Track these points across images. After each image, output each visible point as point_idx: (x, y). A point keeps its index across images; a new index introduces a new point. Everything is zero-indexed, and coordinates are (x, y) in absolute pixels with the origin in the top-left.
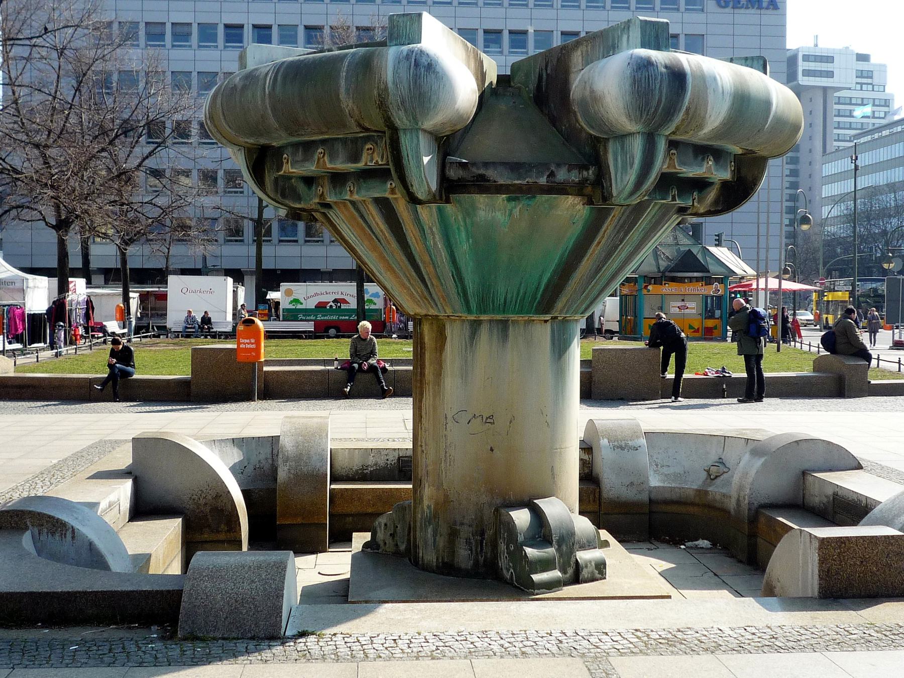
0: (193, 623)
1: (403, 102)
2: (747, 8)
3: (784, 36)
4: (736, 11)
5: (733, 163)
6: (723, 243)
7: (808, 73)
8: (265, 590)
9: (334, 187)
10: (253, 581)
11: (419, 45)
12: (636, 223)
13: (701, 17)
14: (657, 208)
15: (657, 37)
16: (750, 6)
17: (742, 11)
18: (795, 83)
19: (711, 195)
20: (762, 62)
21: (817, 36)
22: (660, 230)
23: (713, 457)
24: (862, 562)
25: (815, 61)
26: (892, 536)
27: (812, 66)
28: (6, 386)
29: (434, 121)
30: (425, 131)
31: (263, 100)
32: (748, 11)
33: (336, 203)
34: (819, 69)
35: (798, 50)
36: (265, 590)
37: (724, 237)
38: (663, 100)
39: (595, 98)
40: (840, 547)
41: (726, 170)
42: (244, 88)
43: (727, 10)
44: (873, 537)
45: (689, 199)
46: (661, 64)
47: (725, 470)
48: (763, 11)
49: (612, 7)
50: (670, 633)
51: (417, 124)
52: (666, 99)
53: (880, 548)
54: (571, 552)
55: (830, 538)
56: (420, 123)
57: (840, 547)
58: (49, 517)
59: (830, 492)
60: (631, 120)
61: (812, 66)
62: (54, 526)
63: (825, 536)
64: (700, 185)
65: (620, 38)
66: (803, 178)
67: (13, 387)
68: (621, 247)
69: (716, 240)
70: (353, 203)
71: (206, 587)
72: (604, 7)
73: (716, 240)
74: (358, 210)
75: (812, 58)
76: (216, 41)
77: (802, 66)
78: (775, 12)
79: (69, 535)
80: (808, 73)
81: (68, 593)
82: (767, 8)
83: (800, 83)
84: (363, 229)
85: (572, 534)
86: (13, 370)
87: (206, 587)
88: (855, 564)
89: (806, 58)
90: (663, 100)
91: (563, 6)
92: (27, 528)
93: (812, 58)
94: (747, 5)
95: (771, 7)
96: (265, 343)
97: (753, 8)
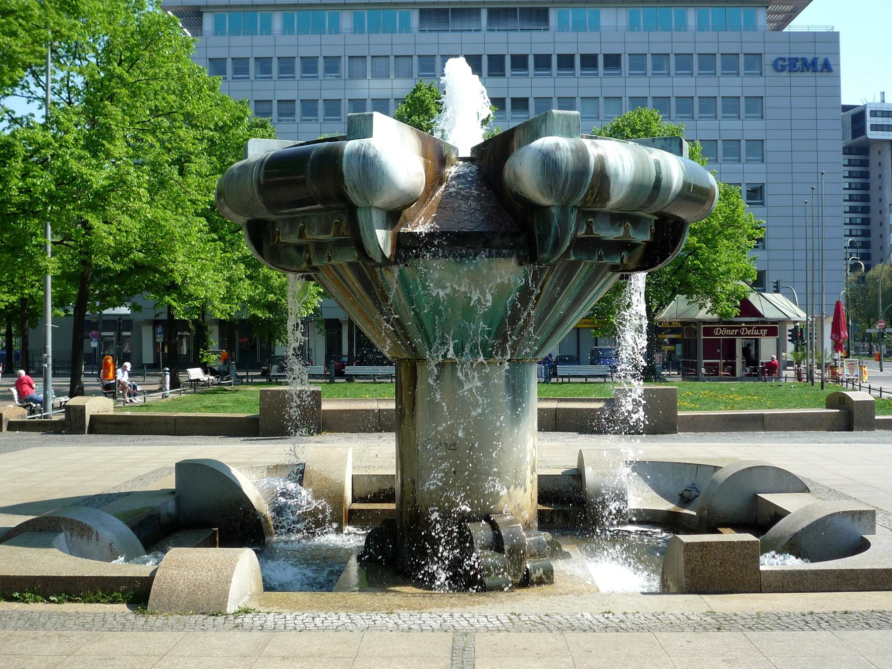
0: (159, 601)
1: (355, 187)
2: (803, 71)
3: (839, 96)
4: (793, 74)
5: (653, 228)
6: (781, 290)
7: (875, 127)
8: (218, 577)
9: (317, 254)
10: (209, 570)
11: (365, 141)
12: (572, 278)
13: (760, 81)
14: (588, 266)
15: (569, 126)
16: (805, 69)
17: (799, 74)
18: (864, 137)
19: (638, 253)
20: (678, 142)
21: (883, 93)
22: (595, 286)
23: (687, 483)
24: (721, 563)
25: (882, 117)
26: (748, 542)
27: (880, 121)
28: (105, 423)
29: (383, 200)
30: (377, 208)
31: (252, 186)
32: (803, 74)
33: (321, 266)
34: (887, 123)
35: (865, 106)
36: (218, 577)
37: (781, 284)
38: (569, 178)
39: (517, 177)
40: (702, 551)
41: (645, 233)
42: (239, 175)
43: (784, 74)
44: (730, 542)
45: (617, 258)
46: (567, 149)
47: (697, 494)
48: (818, 74)
49: (676, 74)
50: (539, 617)
51: (368, 203)
52: (572, 178)
53: (737, 552)
54: (521, 561)
55: (693, 543)
56: (370, 202)
57: (702, 551)
58: (79, 522)
59: (772, 513)
60: (544, 196)
61: (880, 121)
62: (82, 529)
63: (689, 541)
64: (625, 246)
65: (540, 127)
66: (874, 227)
67: (111, 423)
68: (559, 300)
69: (774, 287)
70: (333, 267)
71: (173, 574)
72: (669, 74)
73: (774, 287)
74: (337, 272)
75: (879, 114)
76: (316, 115)
77: (870, 121)
78: (829, 74)
79: (94, 537)
80: (875, 127)
81: (70, 577)
82: (822, 71)
83: (869, 137)
84: (344, 289)
85: (521, 545)
86: (112, 408)
87: (173, 574)
88: (716, 565)
89: (874, 114)
90: (569, 178)
91: (630, 74)
92: (61, 531)
93: (879, 114)
94: (803, 68)
95: (826, 70)
96: (539, 392)
97: (808, 71)
